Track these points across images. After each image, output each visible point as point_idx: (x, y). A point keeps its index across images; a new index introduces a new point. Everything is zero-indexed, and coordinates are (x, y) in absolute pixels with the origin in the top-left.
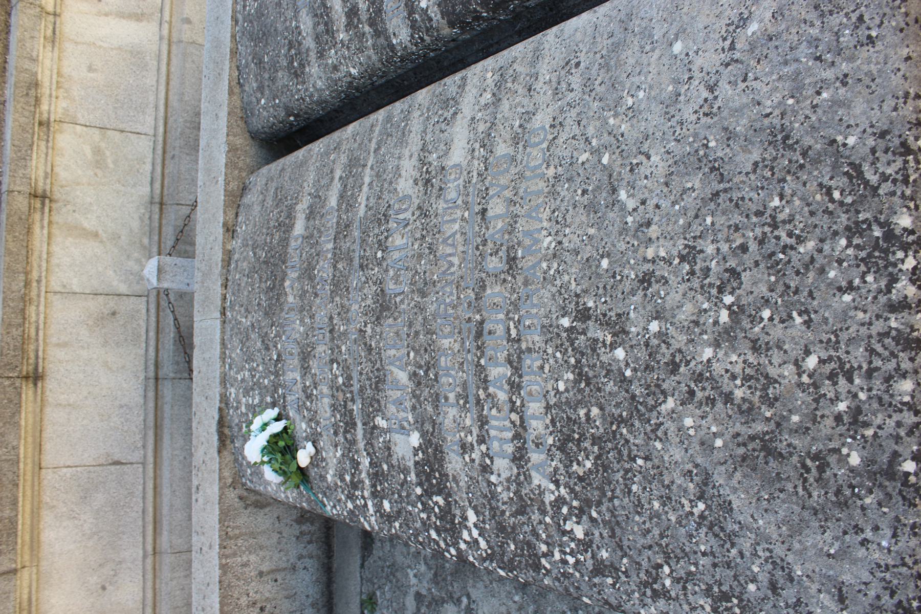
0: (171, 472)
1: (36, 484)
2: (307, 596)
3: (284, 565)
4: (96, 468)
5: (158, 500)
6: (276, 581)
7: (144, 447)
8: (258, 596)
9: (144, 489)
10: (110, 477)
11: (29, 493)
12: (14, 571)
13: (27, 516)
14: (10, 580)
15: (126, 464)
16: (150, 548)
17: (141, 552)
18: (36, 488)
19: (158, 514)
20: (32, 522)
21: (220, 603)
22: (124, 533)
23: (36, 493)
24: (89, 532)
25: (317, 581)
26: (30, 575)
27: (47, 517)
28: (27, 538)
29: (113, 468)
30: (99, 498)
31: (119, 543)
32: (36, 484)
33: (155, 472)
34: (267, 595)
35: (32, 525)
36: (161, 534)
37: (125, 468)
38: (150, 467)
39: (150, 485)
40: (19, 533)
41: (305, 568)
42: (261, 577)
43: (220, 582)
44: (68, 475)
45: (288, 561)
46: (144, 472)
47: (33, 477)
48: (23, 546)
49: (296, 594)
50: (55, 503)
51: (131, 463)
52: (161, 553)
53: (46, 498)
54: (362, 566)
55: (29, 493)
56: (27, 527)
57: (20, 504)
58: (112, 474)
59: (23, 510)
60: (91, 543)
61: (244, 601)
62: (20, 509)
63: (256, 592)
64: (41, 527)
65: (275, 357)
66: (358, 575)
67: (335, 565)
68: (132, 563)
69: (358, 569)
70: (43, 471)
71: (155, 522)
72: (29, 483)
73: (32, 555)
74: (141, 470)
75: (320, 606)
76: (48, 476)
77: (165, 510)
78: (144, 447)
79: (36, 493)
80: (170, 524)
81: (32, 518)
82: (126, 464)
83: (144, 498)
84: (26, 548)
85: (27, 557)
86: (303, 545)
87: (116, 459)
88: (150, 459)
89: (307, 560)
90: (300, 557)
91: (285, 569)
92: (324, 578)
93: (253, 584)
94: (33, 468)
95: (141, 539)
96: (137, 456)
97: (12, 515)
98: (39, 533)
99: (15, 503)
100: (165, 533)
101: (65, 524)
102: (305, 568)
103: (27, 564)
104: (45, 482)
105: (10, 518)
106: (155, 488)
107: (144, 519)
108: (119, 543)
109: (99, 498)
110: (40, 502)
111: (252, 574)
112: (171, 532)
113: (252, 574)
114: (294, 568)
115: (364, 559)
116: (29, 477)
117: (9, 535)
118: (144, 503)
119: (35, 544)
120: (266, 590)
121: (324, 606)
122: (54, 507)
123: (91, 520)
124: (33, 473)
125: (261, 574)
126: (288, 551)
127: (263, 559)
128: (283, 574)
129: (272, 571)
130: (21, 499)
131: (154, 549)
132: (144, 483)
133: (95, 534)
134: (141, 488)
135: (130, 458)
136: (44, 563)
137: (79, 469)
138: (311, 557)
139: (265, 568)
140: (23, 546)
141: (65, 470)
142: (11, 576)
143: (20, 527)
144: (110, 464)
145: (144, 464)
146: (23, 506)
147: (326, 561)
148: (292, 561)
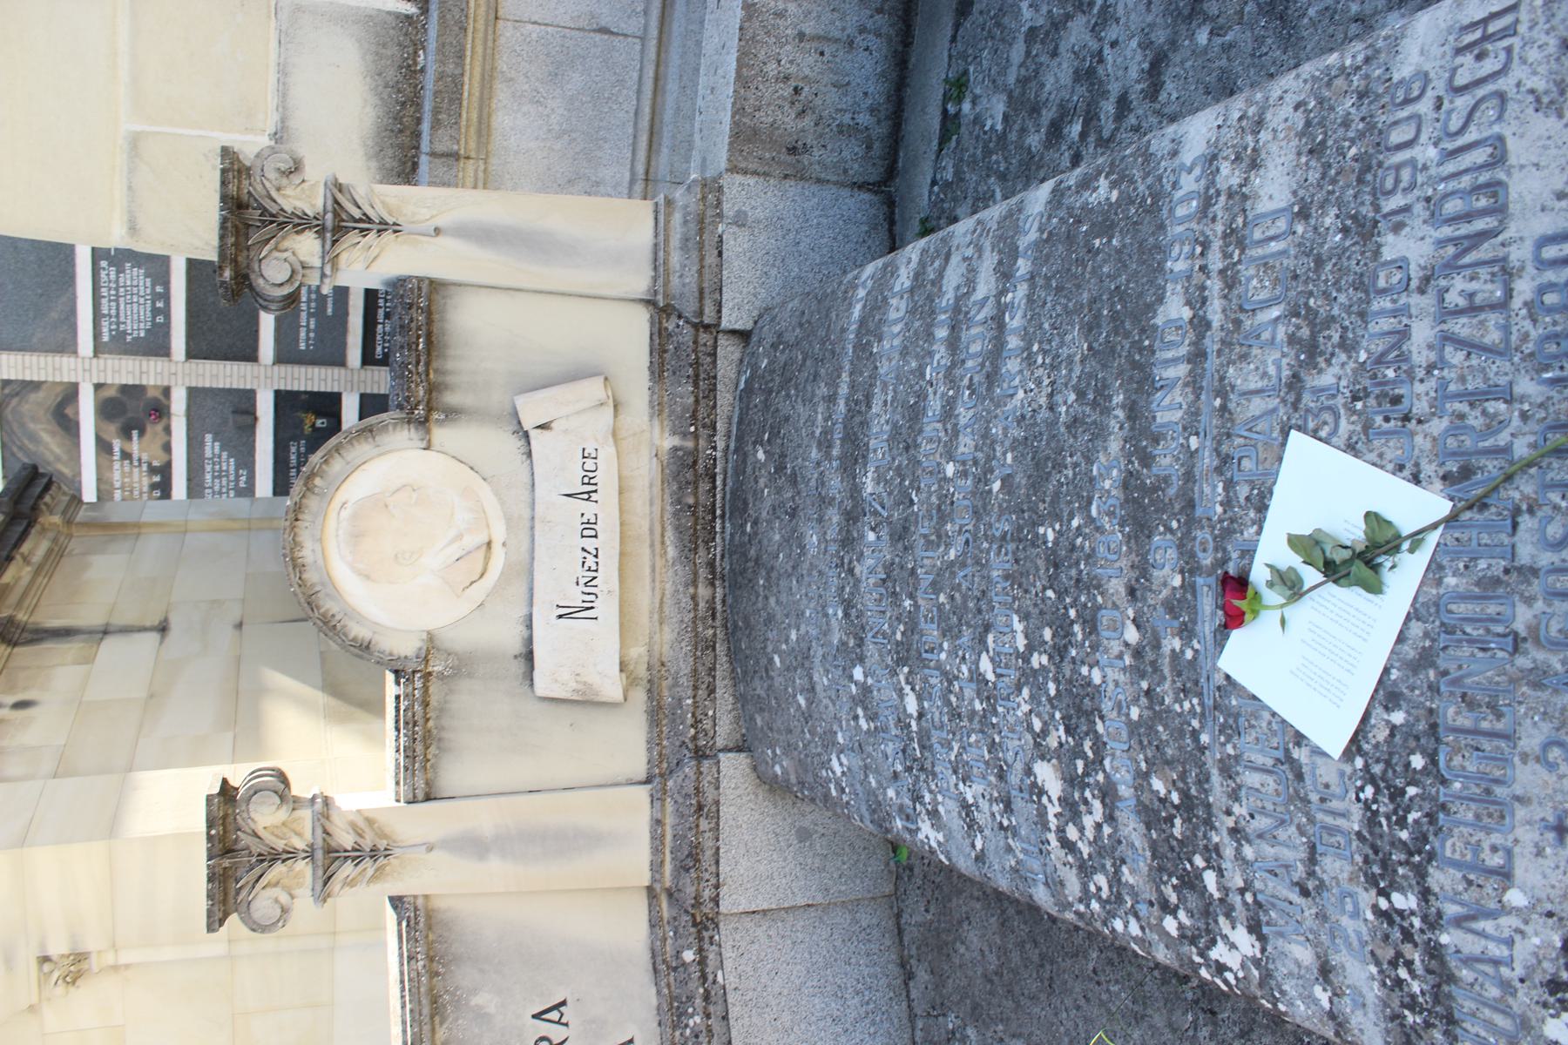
0: (681, 57)
1: (490, 37)
2: (866, 94)
3: (837, 34)
4: (574, 33)
5: (659, 99)
6: (822, 54)
7: (646, 12)
8: (793, 69)
9: (640, 78)
10: (593, 50)
11: (479, 49)
12: (455, 156)
13: (476, 85)
14: (450, 167)
15: (617, 34)
16: (640, 169)
17: (627, 175)
18: (490, 44)
19: (657, 121)
20: (482, 94)
21: (738, 60)
22: (605, 140)
23: (489, 51)
24: (557, 128)
25: (883, 74)
26: (476, 171)
27: (502, 94)
28: (474, 116)
29: (598, 37)
30: (575, 80)
31: (599, 154)
32: (490, 37)
33: (658, 55)
34: (807, 71)
35: (481, 98)
36: (658, 152)
37: (616, 40)
38: (652, 44)
39: (650, 73)
40: (465, 103)
41: (866, 49)
42: (801, 41)
43: (741, 29)
44: (534, 36)
45: (843, 29)
46: (642, 51)
47: (487, 25)
48: (468, 127)
49: (848, 84)
50: (513, 74)
51: (626, 36)
52: (656, 181)
53: (502, 65)
54: (954, 39)
55: (479, 49)
56: (475, 99)
57: (468, 60)
58: (595, 46)
59: (472, 69)
60: (558, 146)
61: (771, 68)
62: (467, 67)
63: (791, 62)
64: (494, 106)
65: (990, 638)
66: (946, 54)
67: (913, 60)
68: (615, 187)
69: (947, 45)
70: (501, 23)
71: (651, 134)
72: (480, 35)
73: (479, 143)
74: (638, 47)
75: (882, 115)
76: (506, 31)
77: (668, 115)
78: (646, 12)
79: (489, 51)
80: (674, 137)
81: (482, 87)
82: (617, 34)
83: (639, 92)
84: (472, 130)
85: (472, 145)
86: (869, 12)
87: (603, 24)
88: (654, 32)
89: (871, 37)
90: (862, 30)
91: (837, 41)
92: (894, 75)
93: (788, 47)
94: (488, 14)
95: (629, 155)
96: (634, 25)
97: (457, 72)
98: (489, 116)
99: (461, 56)
100: (665, 150)
101: (525, 109)
102: (866, 49)
103: (473, 154)
104: (502, 40)
105: (453, 76)
106: (656, 79)
107: (636, 124)
108: (599, 154)
109: (575, 80)
110: (493, 69)
111: (789, 32)
112: (673, 149)
113: (789, 32)
114: (851, 44)
115: (957, 26)
116: (481, 25)
117: (451, 101)
118: (638, 100)
119: (484, 129)
120: (806, 63)
121: (887, 118)
122: (512, 79)
123: (561, 111)
124: (487, 21)
125: (801, 36)
126: (844, 14)
127: (807, 13)
128: (834, 47)
129: (818, 38)
130: (468, 53)
131: (647, 173)
132: (641, 70)
133: (564, 132)
134: (635, 75)
135: (623, 27)
136: (493, 161)
137: (549, 29)
138: (878, 35)
139: (809, 28)
140: (468, 127)
141: (530, 27)
142: (451, 161)
143: (466, 94)
144: (594, 31)
145: (643, 39)
146: (472, 69)
147: (900, 49)
148: (849, 31)
